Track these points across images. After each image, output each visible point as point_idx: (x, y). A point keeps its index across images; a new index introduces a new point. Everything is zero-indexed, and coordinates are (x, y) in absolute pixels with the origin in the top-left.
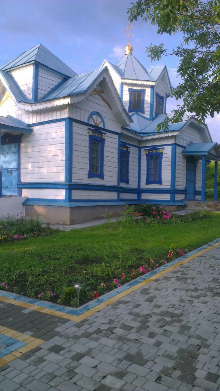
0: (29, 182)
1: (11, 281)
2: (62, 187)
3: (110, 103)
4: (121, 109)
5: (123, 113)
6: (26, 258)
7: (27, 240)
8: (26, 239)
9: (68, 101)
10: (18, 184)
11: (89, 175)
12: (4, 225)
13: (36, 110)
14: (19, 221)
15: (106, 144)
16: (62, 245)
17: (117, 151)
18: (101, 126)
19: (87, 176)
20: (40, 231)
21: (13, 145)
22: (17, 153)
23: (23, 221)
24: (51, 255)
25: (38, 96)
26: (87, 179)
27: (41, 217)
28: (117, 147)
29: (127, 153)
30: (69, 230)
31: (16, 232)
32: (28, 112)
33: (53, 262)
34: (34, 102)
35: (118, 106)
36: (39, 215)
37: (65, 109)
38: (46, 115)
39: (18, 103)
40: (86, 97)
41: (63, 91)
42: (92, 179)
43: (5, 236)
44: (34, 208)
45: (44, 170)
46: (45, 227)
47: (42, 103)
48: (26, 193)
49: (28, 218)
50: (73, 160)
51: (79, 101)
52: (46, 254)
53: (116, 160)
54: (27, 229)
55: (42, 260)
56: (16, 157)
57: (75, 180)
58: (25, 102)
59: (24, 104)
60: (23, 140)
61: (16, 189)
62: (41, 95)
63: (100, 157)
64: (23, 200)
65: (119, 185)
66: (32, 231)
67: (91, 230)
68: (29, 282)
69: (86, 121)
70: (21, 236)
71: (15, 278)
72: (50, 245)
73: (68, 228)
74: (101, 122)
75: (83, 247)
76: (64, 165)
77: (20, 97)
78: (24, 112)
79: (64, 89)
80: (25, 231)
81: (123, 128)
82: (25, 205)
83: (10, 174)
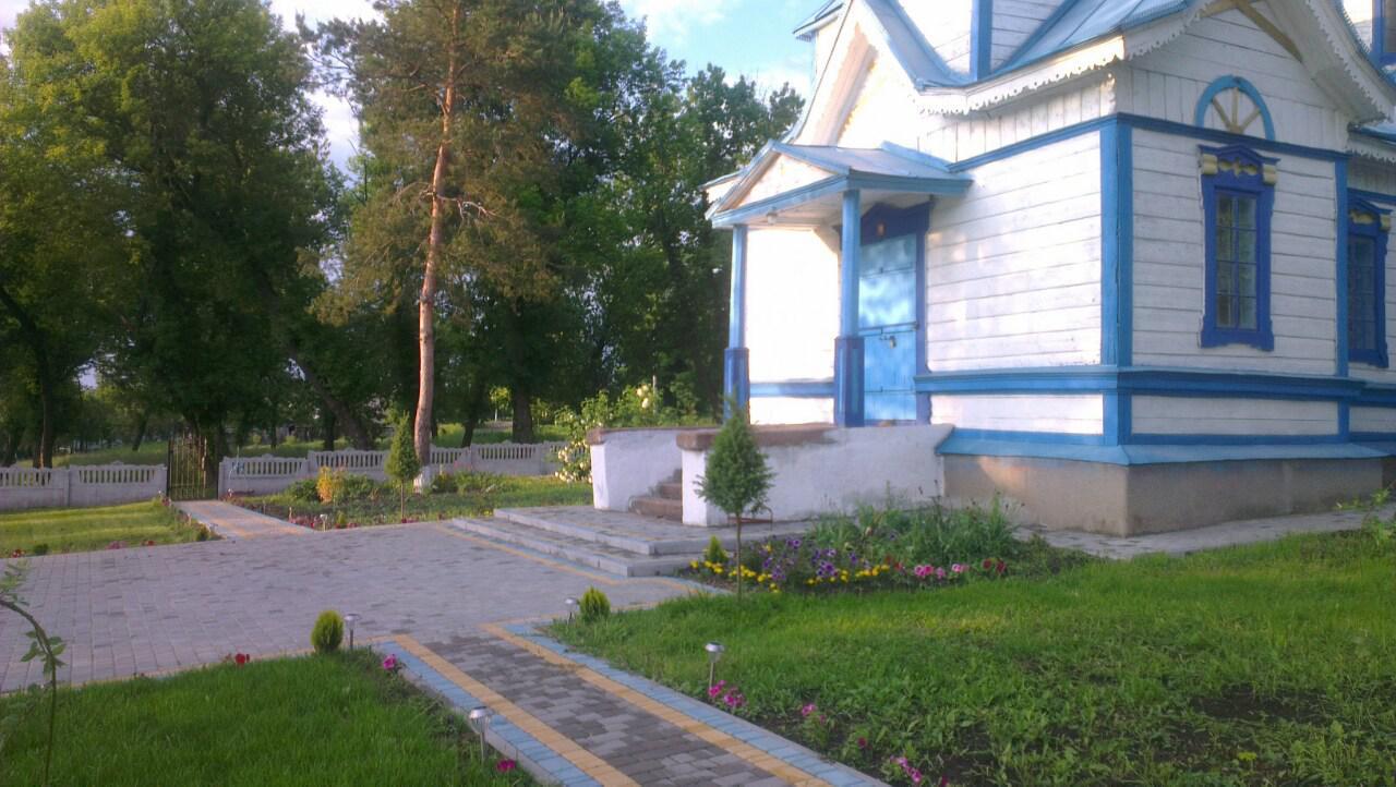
0: (958, 371)
1: (933, 752)
2: (1092, 384)
3: (1292, 35)
4: (1344, 51)
5: (1358, 66)
6: (973, 662)
7: (965, 588)
8: (960, 580)
9: (1115, 49)
10: (917, 380)
11: (1204, 333)
12: (874, 526)
13: (984, 106)
14: (925, 513)
15: (1281, 201)
16: (1113, 622)
17: (1329, 230)
18: (1256, 130)
19: (1196, 339)
20: (1008, 554)
21: (900, 243)
22: (914, 270)
23: (939, 514)
24: (1075, 661)
25: (993, 56)
26: (1196, 350)
27: (1009, 501)
28: (1331, 209)
29: (1374, 238)
30: (1130, 557)
31: (919, 553)
32: (956, 119)
33: (1090, 692)
34: (976, 79)
35: (1331, 42)
36: (999, 493)
37: (1100, 84)
38: (1024, 118)
39: (919, 91)
40: (1188, 24)
41: (1088, 21)
42: (1220, 351)
43: (885, 567)
44: (979, 467)
45: (1006, 325)
46: (1026, 540)
47: (1009, 77)
48: (948, 411)
49: (958, 503)
50: (1136, 278)
51: (1161, 43)
52: (1054, 653)
53: (1330, 268)
54: (960, 545)
55: (1040, 677)
56: (908, 283)
57: (1145, 357)
58: (944, 86)
59: (939, 91)
60: (935, 220)
61: (912, 398)
62: (1001, 49)
63: (1252, 257)
64: (938, 437)
65: (1346, 375)
66: (977, 551)
67: (1229, 564)
68: (1003, 768)
69: (1189, 120)
70: (939, 569)
71: (944, 741)
72: (1062, 614)
73: (1124, 550)
74: (1252, 118)
75: (1213, 637)
76: (1099, 299)
77: (929, 71)
78: (937, 122)
79: (1094, 12)
80: (952, 552)
81: (1356, 132)
82: (946, 455)
83: (891, 344)
